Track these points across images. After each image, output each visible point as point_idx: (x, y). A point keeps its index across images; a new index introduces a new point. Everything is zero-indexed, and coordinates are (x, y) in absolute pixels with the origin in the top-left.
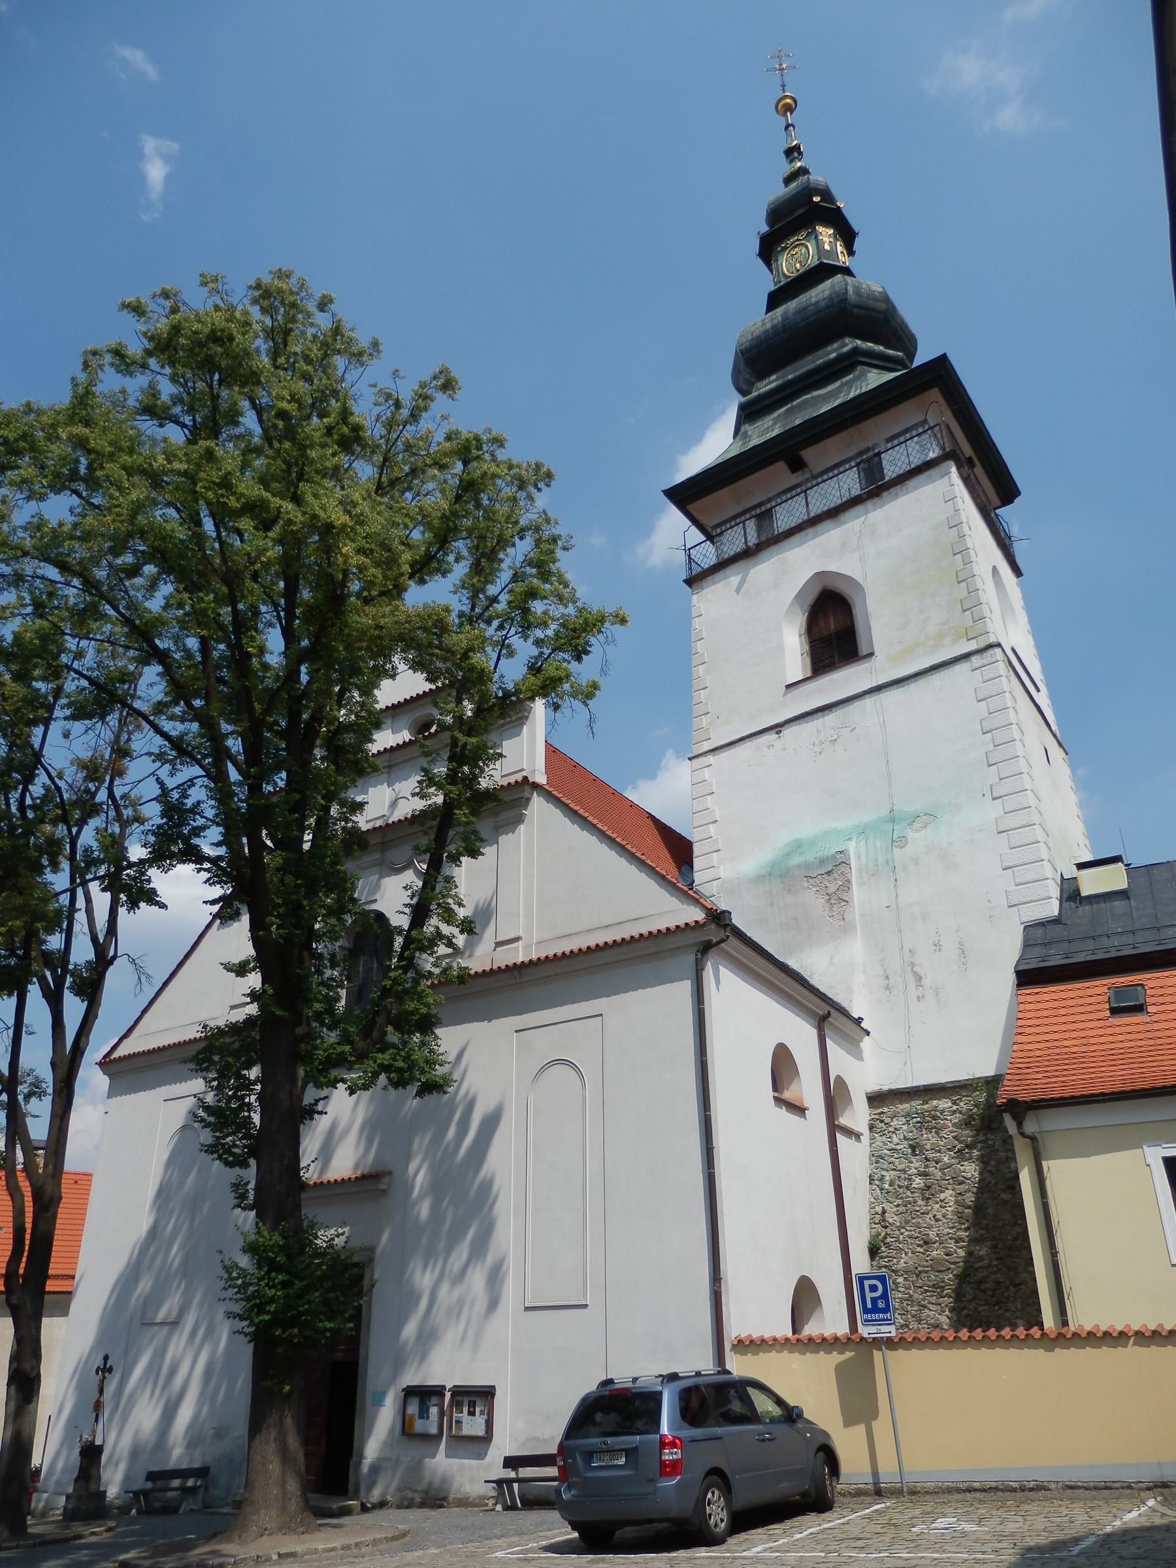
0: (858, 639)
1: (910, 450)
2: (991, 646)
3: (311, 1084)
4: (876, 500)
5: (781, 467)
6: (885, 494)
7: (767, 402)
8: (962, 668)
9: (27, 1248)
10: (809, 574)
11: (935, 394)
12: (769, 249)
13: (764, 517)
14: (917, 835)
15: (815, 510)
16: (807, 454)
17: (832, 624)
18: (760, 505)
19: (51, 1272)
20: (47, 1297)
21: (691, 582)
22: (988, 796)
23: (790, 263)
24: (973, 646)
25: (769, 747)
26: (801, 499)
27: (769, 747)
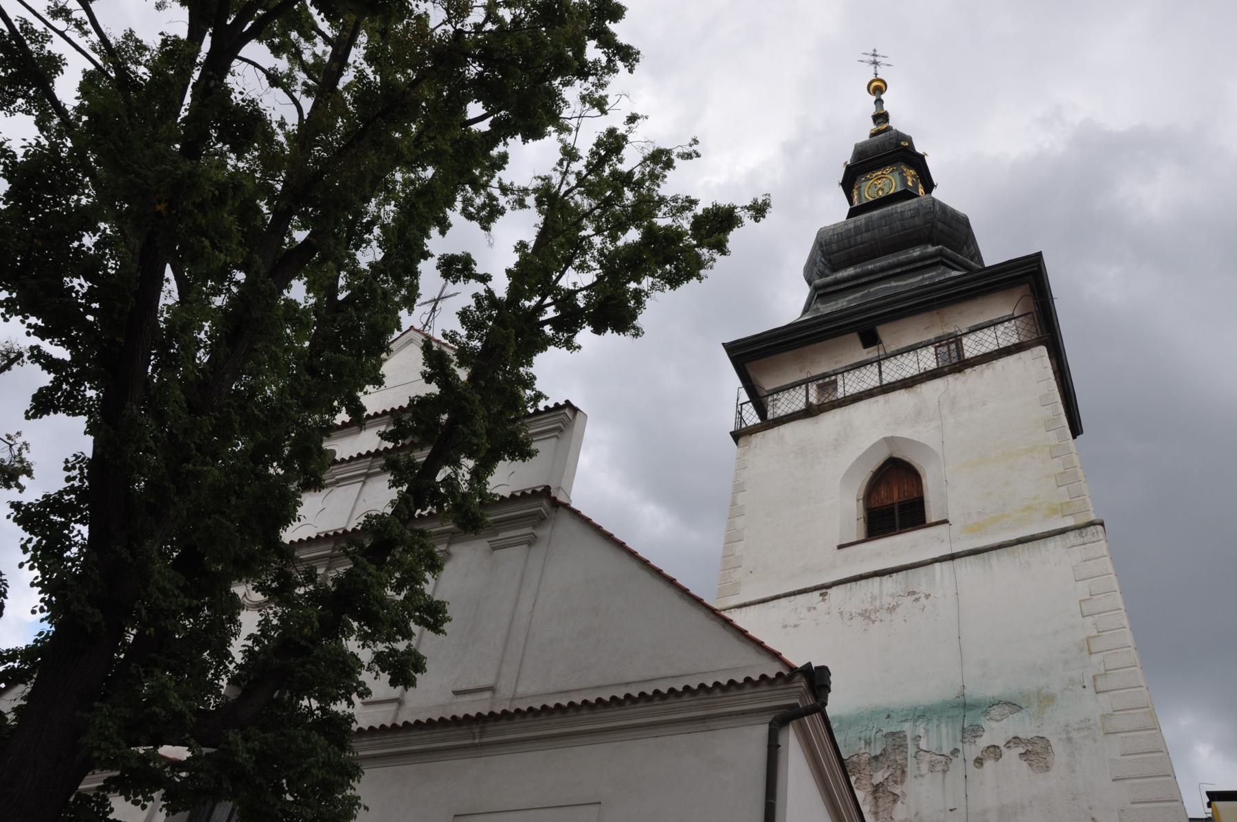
0: (926, 504)
1: (999, 333)
2: (1092, 524)
3: (612, 26)
4: (957, 375)
5: (855, 338)
6: (968, 371)
7: (842, 286)
8: (1053, 544)
9: (189, 90)
10: (876, 437)
11: (1024, 289)
12: (849, 182)
13: (826, 383)
14: (994, 724)
15: (888, 378)
16: (884, 332)
17: (894, 495)
18: (823, 376)
19: (240, 54)
20: (236, 62)
21: (737, 436)
22: (1090, 691)
23: (871, 188)
24: (1070, 522)
25: (809, 610)
26: (874, 369)
27: (809, 610)
